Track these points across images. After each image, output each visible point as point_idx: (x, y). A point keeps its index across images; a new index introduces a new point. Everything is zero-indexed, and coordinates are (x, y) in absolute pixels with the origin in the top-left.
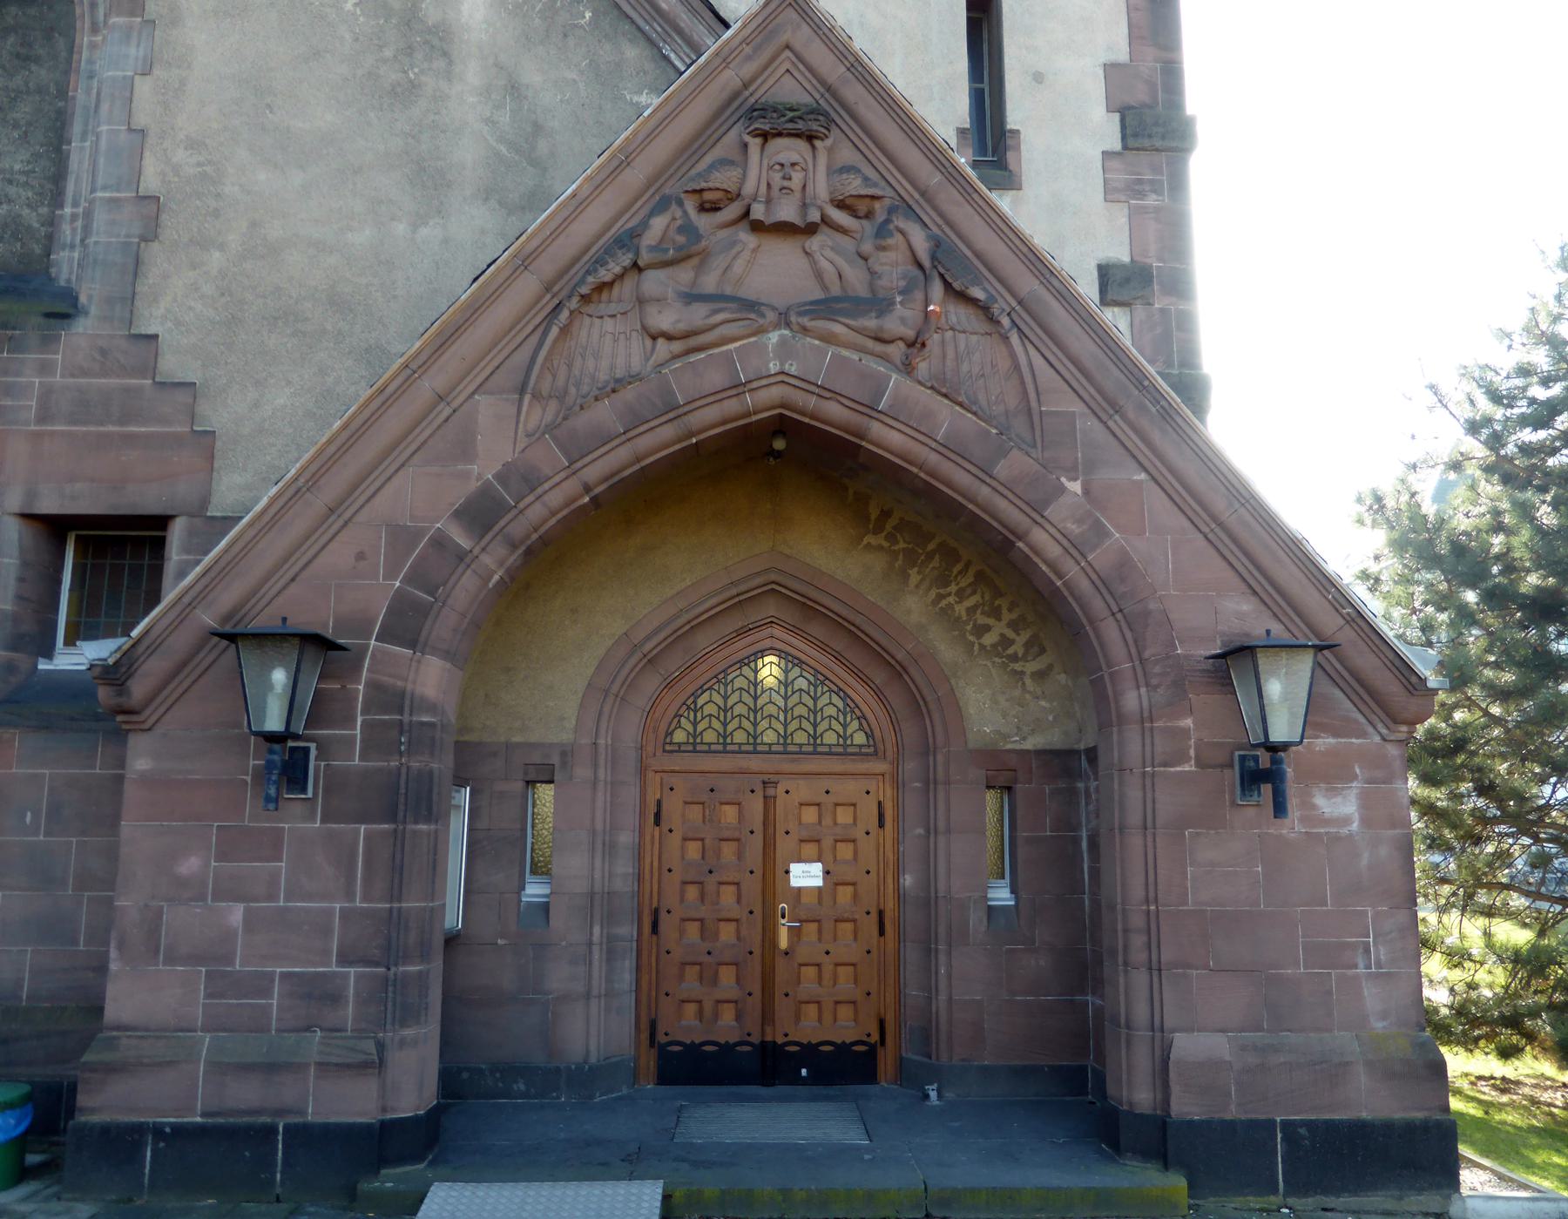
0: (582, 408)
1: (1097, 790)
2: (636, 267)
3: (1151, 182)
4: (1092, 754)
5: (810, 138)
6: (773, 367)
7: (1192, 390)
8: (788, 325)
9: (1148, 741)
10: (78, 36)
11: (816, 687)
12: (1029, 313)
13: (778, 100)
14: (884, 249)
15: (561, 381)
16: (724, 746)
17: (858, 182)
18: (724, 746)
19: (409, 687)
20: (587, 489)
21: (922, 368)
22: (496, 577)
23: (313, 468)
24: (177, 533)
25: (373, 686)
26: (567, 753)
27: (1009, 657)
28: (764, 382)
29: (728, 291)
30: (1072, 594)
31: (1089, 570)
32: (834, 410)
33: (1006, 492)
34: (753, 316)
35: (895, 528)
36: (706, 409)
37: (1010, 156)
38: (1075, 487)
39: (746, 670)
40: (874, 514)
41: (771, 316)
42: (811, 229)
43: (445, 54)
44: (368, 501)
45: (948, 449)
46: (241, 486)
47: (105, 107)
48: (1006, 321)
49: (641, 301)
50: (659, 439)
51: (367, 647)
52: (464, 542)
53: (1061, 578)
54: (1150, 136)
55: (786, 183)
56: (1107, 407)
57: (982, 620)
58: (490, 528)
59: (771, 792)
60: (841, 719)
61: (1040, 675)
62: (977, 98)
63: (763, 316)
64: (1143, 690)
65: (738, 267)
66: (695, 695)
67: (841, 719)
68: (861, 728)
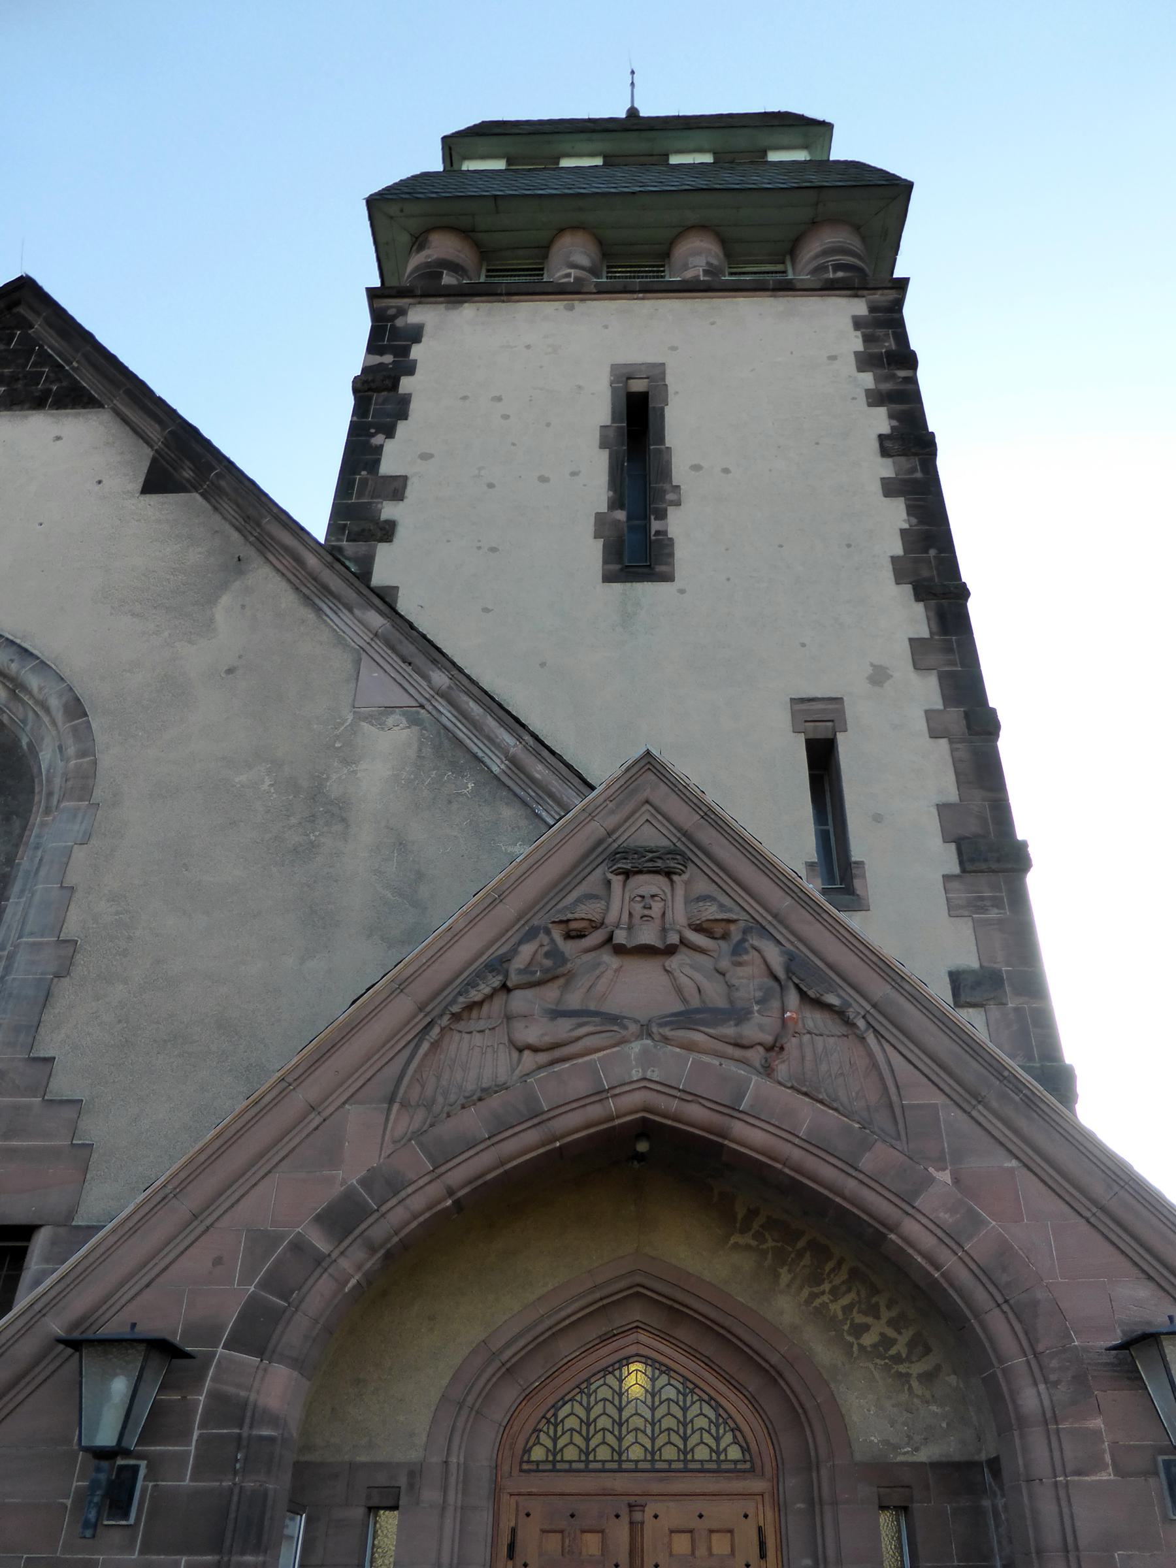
0: (448, 1116)
1: (1005, 1507)
2: (505, 988)
3: (990, 898)
4: (994, 1465)
5: (669, 874)
6: (636, 1074)
7: (1059, 1081)
8: (650, 1035)
9: (1055, 1445)
10: (33, 816)
11: (685, 1395)
12: (913, 1042)
13: (638, 844)
14: (740, 964)
15: (429, 1091)
16: (587, 1464)
17: (714, 908)
18: (587, 1464)
19: (253, 1397)
20: (451, 1192)
21: (782, 1070)
22: (353, 1282)
23: (182, 1175)
24: (39, 1243)
25: (214, 1396)
26: (415, 1473)
27: (892, 1357)
28: (627, 1088)
29: (592, 1007)
30: (952, 1285)
31: (967, 1260)
32: (695, 1112)
33: (873, 1184)
34: (615, 1028)
35: (762, 1226)
36: (570, 1115)
37: (857, 883)
38: (945, 1177)
39: (610, 1379)
40: (741, 1213)
41: (633, 1028)
42: (670, 950)
43: (343, 820)
44: (232, 1206)
45: (816, 1145)
46: (107, 1197)
47: (42, 873)
48: (861, 1023)
49: (509, 1018)
50: (523, 1143)
51: (214, 1354)
52: (321, 1243)
53: (938, 1269)
54: (986, 860)
55: (646, 912)
56: (970, 1098)
57: (860, 1319)
58: (350, 1233)
59: (638, 1516)
60: (713, 1431)
61: (928, 1378)
62: (823, 839)
63: (626, 1028)
64: (1042, 1387)
65: (601, 986)
66: (556, 1407)
67: (713, 1431)
68: (735, 1441)
